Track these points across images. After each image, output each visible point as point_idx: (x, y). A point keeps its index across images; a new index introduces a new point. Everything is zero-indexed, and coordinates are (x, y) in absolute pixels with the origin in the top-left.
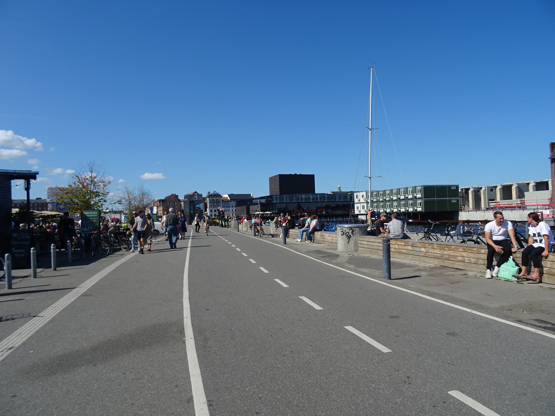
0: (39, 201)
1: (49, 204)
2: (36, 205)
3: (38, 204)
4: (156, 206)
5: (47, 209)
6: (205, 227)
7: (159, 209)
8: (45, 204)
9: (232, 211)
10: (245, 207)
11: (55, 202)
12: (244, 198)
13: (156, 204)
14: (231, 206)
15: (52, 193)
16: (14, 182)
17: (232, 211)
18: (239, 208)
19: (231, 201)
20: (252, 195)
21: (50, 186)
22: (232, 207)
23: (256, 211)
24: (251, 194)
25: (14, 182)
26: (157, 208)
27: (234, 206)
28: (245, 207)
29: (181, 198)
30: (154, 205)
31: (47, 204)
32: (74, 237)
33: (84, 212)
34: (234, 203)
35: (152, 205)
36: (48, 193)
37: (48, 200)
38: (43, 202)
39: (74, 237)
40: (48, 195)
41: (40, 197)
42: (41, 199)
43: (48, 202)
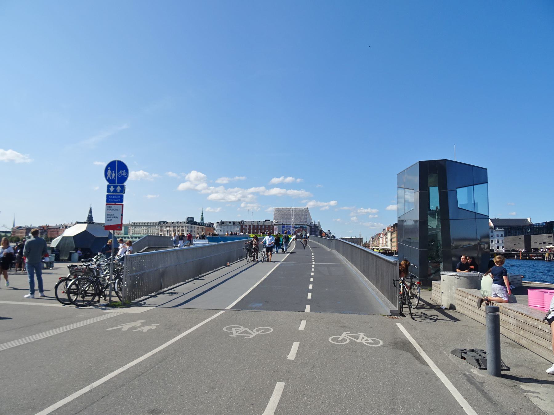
0: (267, 223)
1: (275, 227)
2: (263, 227)
3: (265, 226)
4: (390, 231)
5: (118, 225)
6: (111, 269)
7: (393, 236)
8: (272, 226)
9: (498, 242)
10: (523, 237)
11: (281, 225)
12: (516, 224)
13: (390, 230)
14: (495, 235)
15: (278, 214)
16: (119, 191)
17: (498, 242)
18: (510, 238)
19: (495, 229)
20: (529, 219)
21: (277, 207)
22: (498, 236)
23: (544, 243)
24: (527, 219)
25: (119, 191)
26: (391, 235)
27: (500, 235)
28: (523, 237)
29: (124, 194)
30: (388, 230)
31: (273, 226)
32: (116, 269)
33: (289, 236)
34: (501, 232)
35: (387, 231)
36: (275, 214)
37: (274, 223)
38: (270, 224)
39: (116, 269)
40: (275, 217)
41: (268, 219)
42: (269, 220)
43: (275, 225)
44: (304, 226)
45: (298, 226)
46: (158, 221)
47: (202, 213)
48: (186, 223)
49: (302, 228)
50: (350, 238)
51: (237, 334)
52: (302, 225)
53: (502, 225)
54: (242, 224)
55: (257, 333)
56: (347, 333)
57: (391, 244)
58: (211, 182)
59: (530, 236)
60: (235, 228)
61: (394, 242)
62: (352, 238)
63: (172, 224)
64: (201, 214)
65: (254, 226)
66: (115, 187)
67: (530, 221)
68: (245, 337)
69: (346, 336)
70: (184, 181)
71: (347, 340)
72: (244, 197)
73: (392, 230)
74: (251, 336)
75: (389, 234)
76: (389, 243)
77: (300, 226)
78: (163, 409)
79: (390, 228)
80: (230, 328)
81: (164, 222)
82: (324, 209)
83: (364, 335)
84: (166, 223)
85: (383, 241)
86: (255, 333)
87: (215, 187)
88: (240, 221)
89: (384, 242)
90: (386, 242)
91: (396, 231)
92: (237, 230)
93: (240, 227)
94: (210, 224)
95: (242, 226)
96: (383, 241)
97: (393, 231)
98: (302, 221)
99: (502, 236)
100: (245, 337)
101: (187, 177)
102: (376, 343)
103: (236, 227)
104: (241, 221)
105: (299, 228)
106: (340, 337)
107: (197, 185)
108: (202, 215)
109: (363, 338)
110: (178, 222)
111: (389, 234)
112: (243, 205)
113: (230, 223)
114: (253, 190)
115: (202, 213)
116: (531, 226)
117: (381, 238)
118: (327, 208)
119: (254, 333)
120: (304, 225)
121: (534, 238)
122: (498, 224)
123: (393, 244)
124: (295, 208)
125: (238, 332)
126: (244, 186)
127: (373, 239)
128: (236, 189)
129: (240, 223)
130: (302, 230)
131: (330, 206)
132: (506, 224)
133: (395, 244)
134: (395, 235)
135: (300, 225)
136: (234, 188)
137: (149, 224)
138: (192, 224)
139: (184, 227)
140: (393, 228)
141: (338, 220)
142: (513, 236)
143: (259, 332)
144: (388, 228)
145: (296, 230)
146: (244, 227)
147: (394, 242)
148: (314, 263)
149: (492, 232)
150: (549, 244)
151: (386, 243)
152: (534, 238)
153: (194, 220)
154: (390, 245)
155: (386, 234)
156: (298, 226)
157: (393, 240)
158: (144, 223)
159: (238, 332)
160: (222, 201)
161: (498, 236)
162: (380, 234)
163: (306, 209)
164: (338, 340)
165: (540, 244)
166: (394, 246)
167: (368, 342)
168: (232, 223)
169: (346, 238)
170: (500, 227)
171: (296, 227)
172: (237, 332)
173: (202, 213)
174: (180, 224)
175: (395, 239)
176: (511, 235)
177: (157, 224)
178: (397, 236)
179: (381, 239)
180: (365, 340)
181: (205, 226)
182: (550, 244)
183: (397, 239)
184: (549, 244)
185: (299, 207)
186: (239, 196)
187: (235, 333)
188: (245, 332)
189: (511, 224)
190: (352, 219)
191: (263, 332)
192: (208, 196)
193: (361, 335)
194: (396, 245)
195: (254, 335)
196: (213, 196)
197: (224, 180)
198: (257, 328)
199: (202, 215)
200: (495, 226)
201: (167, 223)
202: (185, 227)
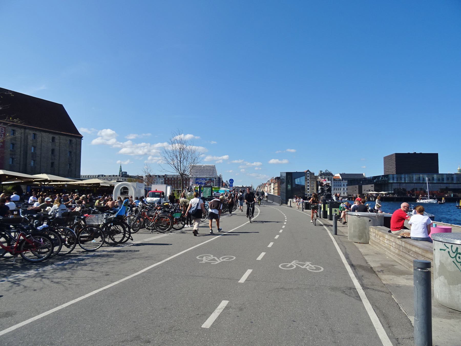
7: (275, 186)
9: (344, 190)
10: (357, 186)
12: (356, 177)
13: (273, 181)
14: (343, 185)
17: (344, 190)
18: (350, 187)
19: (342, 180)
20: (364, 174)
22: (344, 186)
23: (369, 190)
26: (274, 185)
27: (345, 185)
28: (357, 186)
30: (272, 182)
31: (189, 179)
34: (346, 182)
43: (190, 178)
44: (212, 179)
45: (207, 179)
46: (98, 174)
47: (121, 167)
48: (121, 176)
49: (211, 180)
50: (241, 186)
51: (206, 261)
52: (211, 178)
53: (347, 178)
54: (165, 177)
55: (222, 260)
56: (296, 262)
57: (274, 191)
58: (121, 139)
59: (362, 186)
60: (160, 180)
61: (276, 190)
62: (244, 187)
63: (109, 177)
64: (120, 167)
65: (174, 179)
66: (231, 184)
67: (364, 175)
68: (212, 264)
69: (294, 263)
70: (96, 137)
71: (293, 267)
72: (149, 151)
73: (274, 181)
74: (217, 263)
75: (272, 184)
76: (272, 191)
77: (209, 179)
78: (111, 300)
79: (273, 180)
80: (202, 257)
81: (102, 175)
82: (218, 162)
83: (310, 263)
84: (104, 176)
85: (268, 189)
86: (220, 260)
87: (123, 143)
88: (164, 175)
89: (269, 190)
90: (270, 190)
91: (277, 182)
92: (161, 182)
93: (164, 179)
94: (138, 177)
95: (165, 179)
96: (268, 189)
97: (275, 182)
98: (210, 175)
99: (347, 185)
100: (212, 264)
101: (99, 134)
102: (318, 269)
103: (161, 179)
104: (164, 175)
105: (208, 180)
106: (288, 264)
107: (108, 140)
108: (120, 168)
109: (308, 265)
110: (114, 176)
111: (272, 184)
112: (150, 158)
113: (156, 176)
114: (159, 145)
115: (121, 167)
116: (365, 179)
117: (266, 187)
118: (221, 161)
119: (219, 261)
120: (212, 178)
121: (364, 187)
122: (344, 177)
123: (275, 192)
124: (206, 166)
125: (207, 259)
126: (152, 142)
127: (259, 187)
128: (143, 144)
129: (163, 176)
130: (211, 182)
131: (223, 160)
132: (349, 177)
133: (277, 191)
134: (276, 185)
135: (209, 178)
136: (141, 143)
137: (90, 177)
138: (126, 177)
139: (120, 179)
140: (275, 180)
141: (231, 171)
142: (353, 185)
143: (224, 260)
144: (272, 180)
145: (206, 181)
146: (167, 179)
147: (276, 190)
148: (286, 220)
149: (340, 183)
150: (372, 191)
151: (270, 191)
152: (364, 187)
153: (127, 174)
154: (273, 192)
155: (270, 184)
156: (207, 179)
157: (275, 189)
158: (86, 176)
159: (207, 259)
160: (132, 155)
161: (344, 186)
162: (265, 184)
163: (214, 166)
164: (287, 266)
165: (367, 191)
166: (276, 193)
167: (311, 268)
168: (158, 176)
169: (238, 187)
170: (345, 179)
171: (206, 179)
172: (206, 260)
173: (120, 166)
174: (116, 177)
175: (277, 188)
176: (351, 185)
177: (97, 177)
178: (278, 186)
179: (266, 188)
180: (309, 267)
181: (135, 178)
182: (372, 191)
183: (278, 188)
184: (372, 191)
185: (208, 165)
186: (146, 150)
187: (205, 260)
188: (214, 260)
189: (352, 177)
190: (241, 170)
191: (227, 259)
192: (120, 150)
193: (308, 263)
194: (277, 192)
195: (219, 261)
196: (123, 150)
197: (132, 137)
198: (223, 257)
199: (121, 168)
200: (342, 179)
201: (105, 176)
202: (120, 179)
